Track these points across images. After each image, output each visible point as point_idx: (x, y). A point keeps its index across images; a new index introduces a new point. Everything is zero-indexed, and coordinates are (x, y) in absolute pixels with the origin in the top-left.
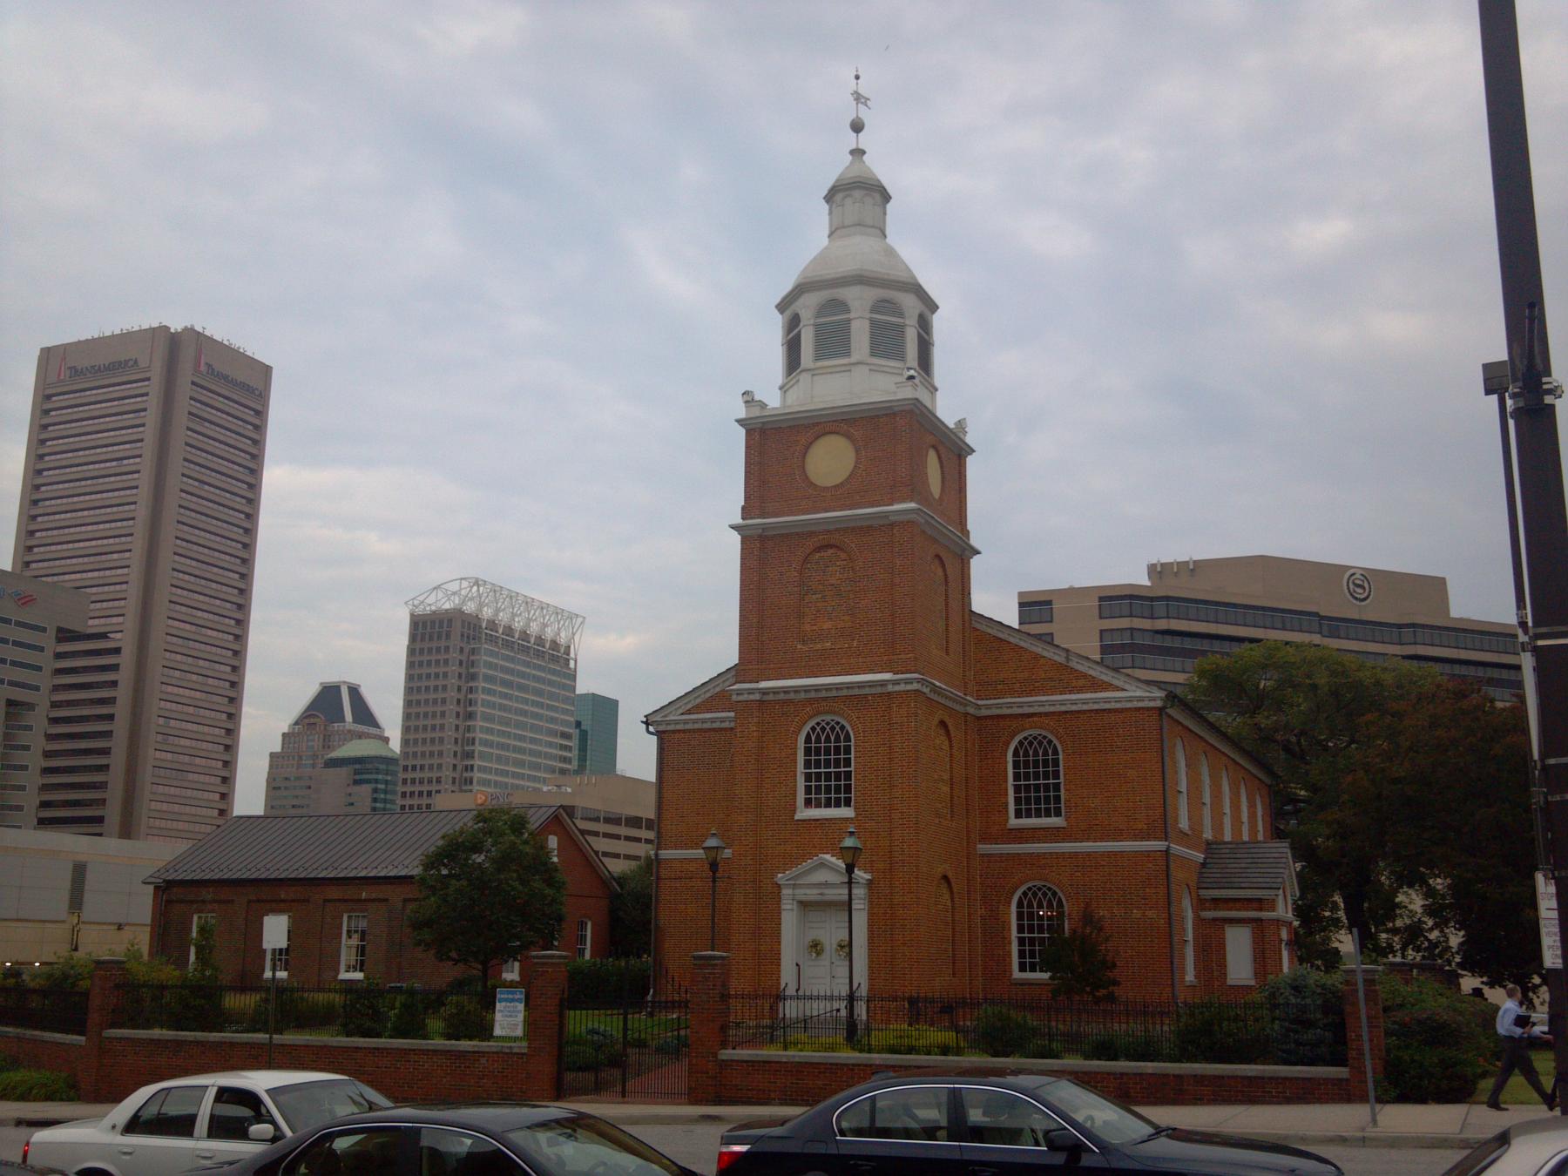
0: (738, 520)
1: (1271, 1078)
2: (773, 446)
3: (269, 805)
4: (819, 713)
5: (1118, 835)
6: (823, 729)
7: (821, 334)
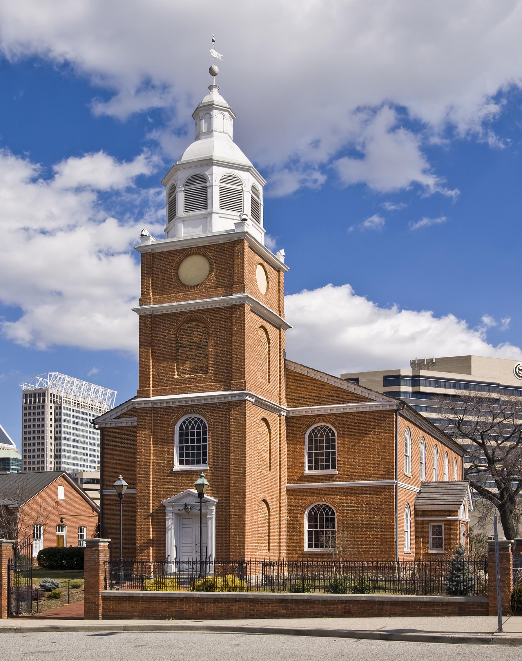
1: (438, 603)
4: (187, 413)
5: (367, 477)
6: (190, 422)
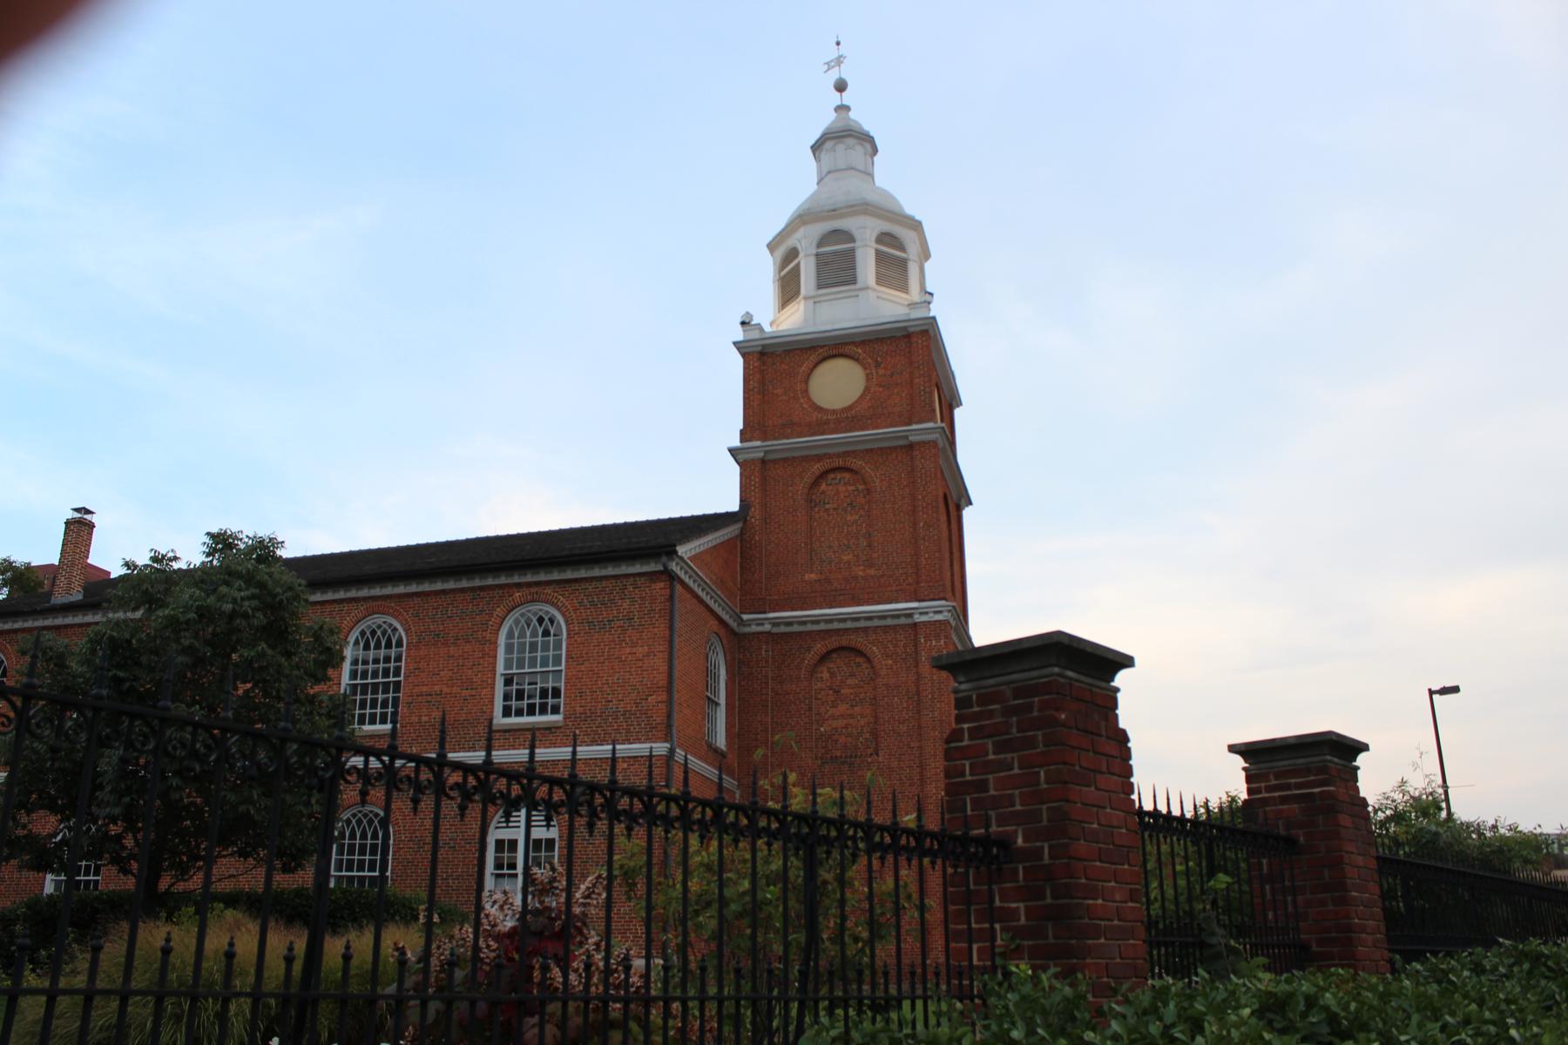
0: (736, 443)
2: (772, 369)
3: (756, 472)
7: (823, 262)
